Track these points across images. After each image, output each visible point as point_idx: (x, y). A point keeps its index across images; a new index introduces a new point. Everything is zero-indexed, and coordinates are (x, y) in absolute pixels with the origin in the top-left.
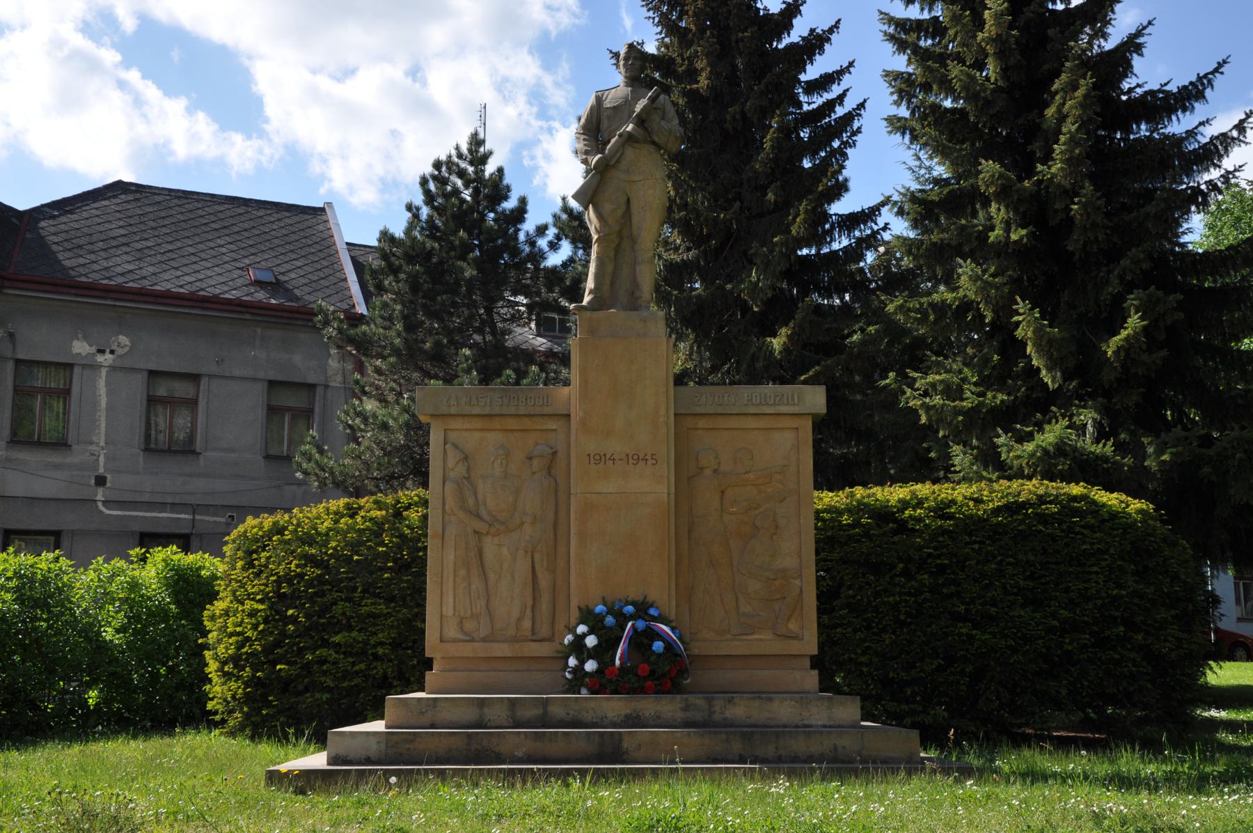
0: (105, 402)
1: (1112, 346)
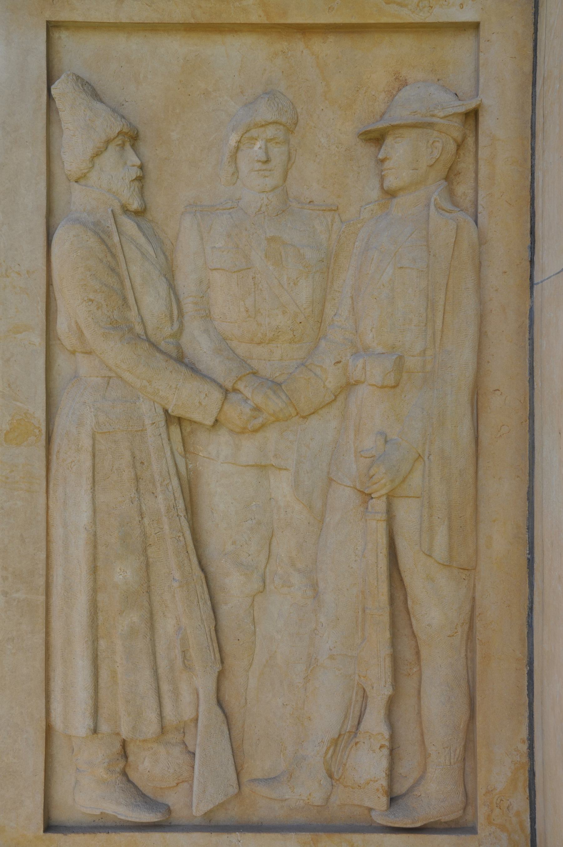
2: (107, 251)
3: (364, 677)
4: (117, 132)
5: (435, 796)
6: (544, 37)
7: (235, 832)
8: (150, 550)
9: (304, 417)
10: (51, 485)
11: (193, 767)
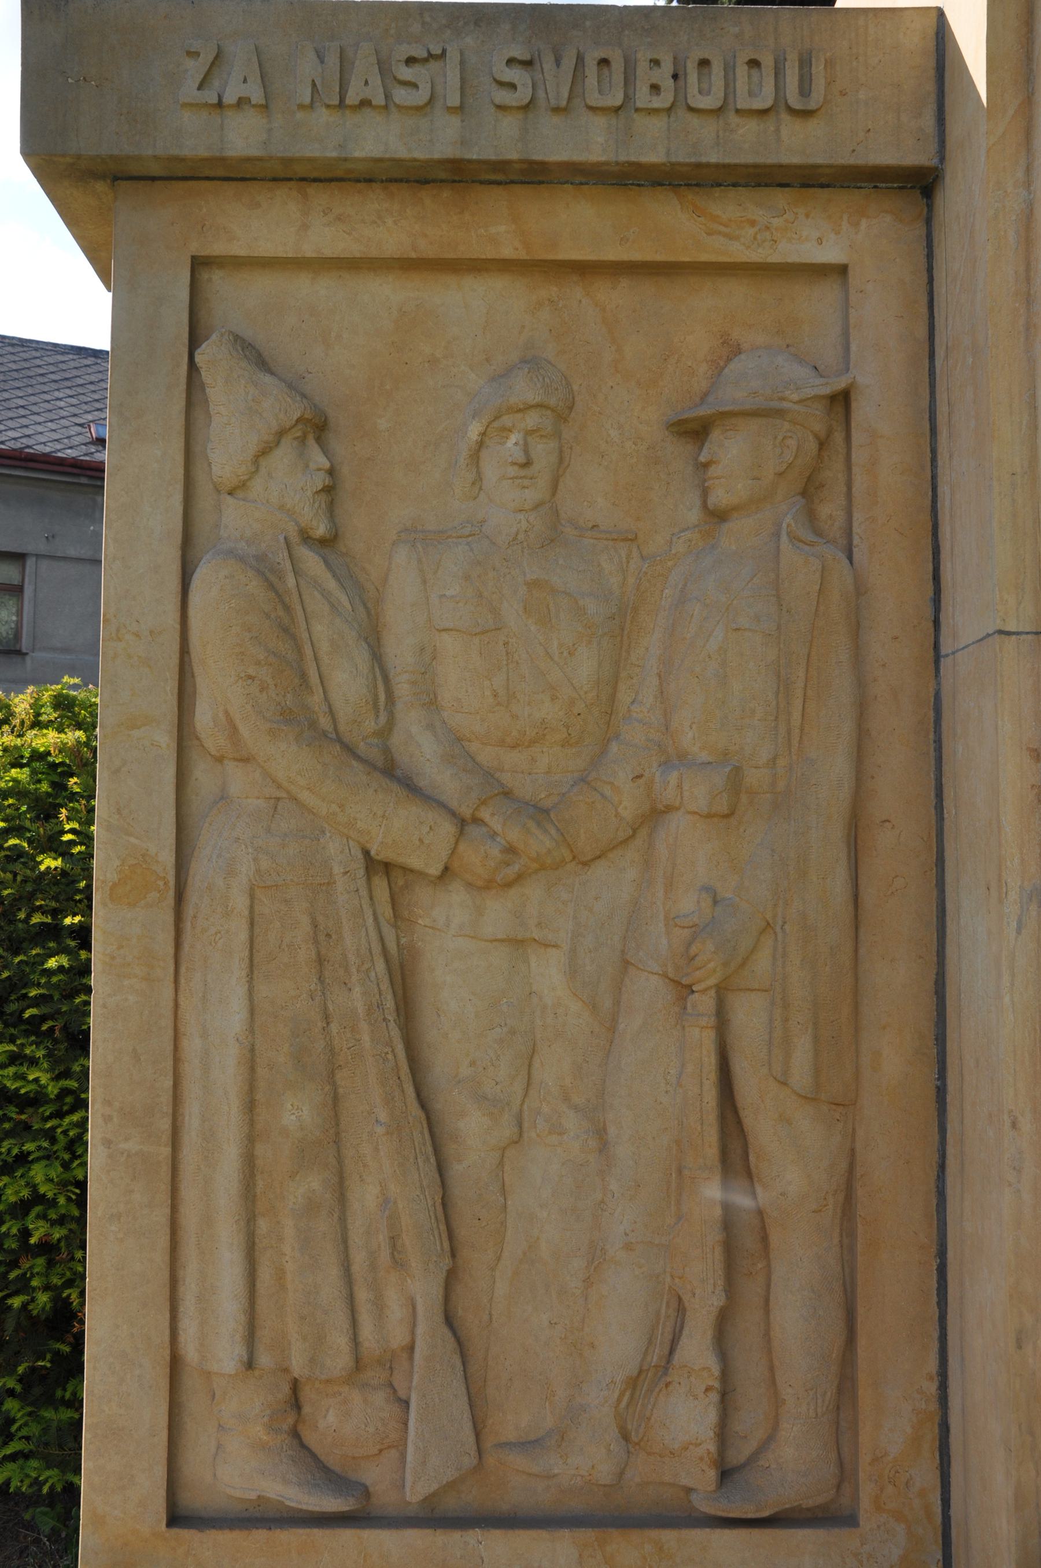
2: (277, 600)
3: (680, 1278)
4: (295, 418)
5: (793, 1466)
6: (944, 290)
7: (474, 1528)
8: (339, 1075)
9: (585, 864)
10: (183, 970)
11: (406, 1424)
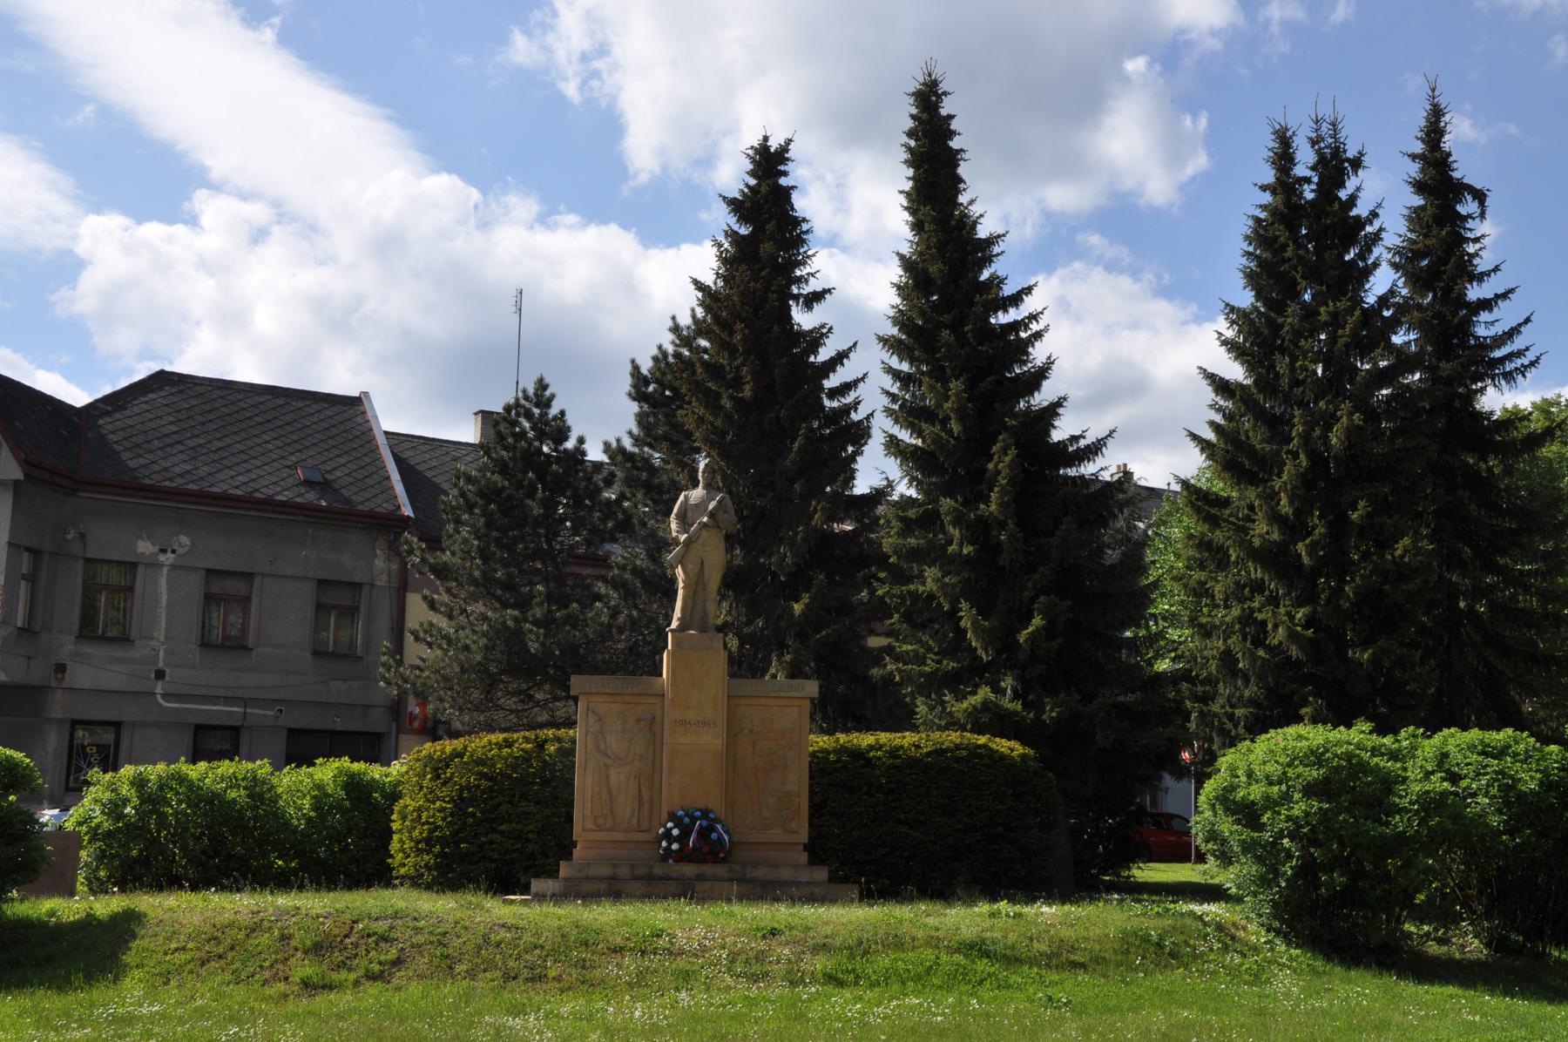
0: (165, 602)
1: (1022, 637)
5: (645, 825)
